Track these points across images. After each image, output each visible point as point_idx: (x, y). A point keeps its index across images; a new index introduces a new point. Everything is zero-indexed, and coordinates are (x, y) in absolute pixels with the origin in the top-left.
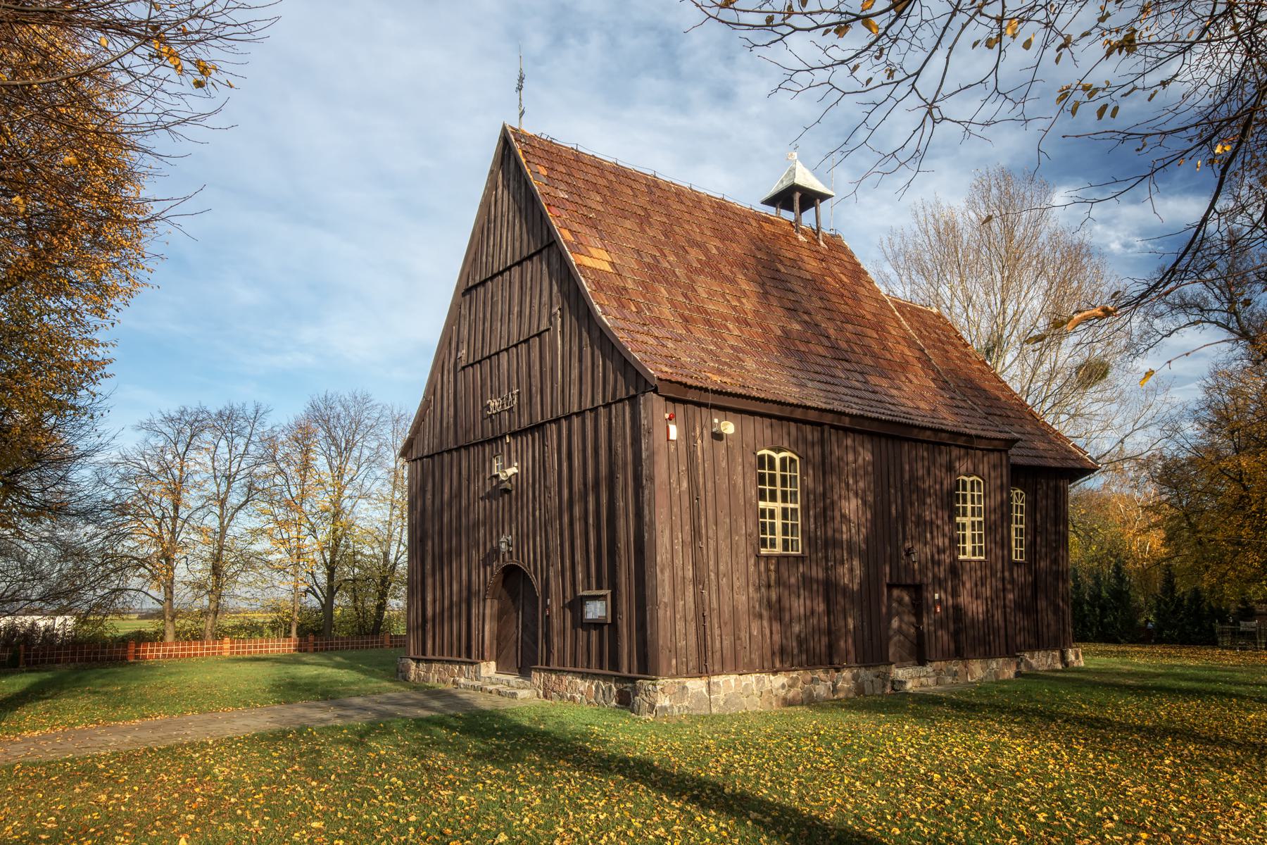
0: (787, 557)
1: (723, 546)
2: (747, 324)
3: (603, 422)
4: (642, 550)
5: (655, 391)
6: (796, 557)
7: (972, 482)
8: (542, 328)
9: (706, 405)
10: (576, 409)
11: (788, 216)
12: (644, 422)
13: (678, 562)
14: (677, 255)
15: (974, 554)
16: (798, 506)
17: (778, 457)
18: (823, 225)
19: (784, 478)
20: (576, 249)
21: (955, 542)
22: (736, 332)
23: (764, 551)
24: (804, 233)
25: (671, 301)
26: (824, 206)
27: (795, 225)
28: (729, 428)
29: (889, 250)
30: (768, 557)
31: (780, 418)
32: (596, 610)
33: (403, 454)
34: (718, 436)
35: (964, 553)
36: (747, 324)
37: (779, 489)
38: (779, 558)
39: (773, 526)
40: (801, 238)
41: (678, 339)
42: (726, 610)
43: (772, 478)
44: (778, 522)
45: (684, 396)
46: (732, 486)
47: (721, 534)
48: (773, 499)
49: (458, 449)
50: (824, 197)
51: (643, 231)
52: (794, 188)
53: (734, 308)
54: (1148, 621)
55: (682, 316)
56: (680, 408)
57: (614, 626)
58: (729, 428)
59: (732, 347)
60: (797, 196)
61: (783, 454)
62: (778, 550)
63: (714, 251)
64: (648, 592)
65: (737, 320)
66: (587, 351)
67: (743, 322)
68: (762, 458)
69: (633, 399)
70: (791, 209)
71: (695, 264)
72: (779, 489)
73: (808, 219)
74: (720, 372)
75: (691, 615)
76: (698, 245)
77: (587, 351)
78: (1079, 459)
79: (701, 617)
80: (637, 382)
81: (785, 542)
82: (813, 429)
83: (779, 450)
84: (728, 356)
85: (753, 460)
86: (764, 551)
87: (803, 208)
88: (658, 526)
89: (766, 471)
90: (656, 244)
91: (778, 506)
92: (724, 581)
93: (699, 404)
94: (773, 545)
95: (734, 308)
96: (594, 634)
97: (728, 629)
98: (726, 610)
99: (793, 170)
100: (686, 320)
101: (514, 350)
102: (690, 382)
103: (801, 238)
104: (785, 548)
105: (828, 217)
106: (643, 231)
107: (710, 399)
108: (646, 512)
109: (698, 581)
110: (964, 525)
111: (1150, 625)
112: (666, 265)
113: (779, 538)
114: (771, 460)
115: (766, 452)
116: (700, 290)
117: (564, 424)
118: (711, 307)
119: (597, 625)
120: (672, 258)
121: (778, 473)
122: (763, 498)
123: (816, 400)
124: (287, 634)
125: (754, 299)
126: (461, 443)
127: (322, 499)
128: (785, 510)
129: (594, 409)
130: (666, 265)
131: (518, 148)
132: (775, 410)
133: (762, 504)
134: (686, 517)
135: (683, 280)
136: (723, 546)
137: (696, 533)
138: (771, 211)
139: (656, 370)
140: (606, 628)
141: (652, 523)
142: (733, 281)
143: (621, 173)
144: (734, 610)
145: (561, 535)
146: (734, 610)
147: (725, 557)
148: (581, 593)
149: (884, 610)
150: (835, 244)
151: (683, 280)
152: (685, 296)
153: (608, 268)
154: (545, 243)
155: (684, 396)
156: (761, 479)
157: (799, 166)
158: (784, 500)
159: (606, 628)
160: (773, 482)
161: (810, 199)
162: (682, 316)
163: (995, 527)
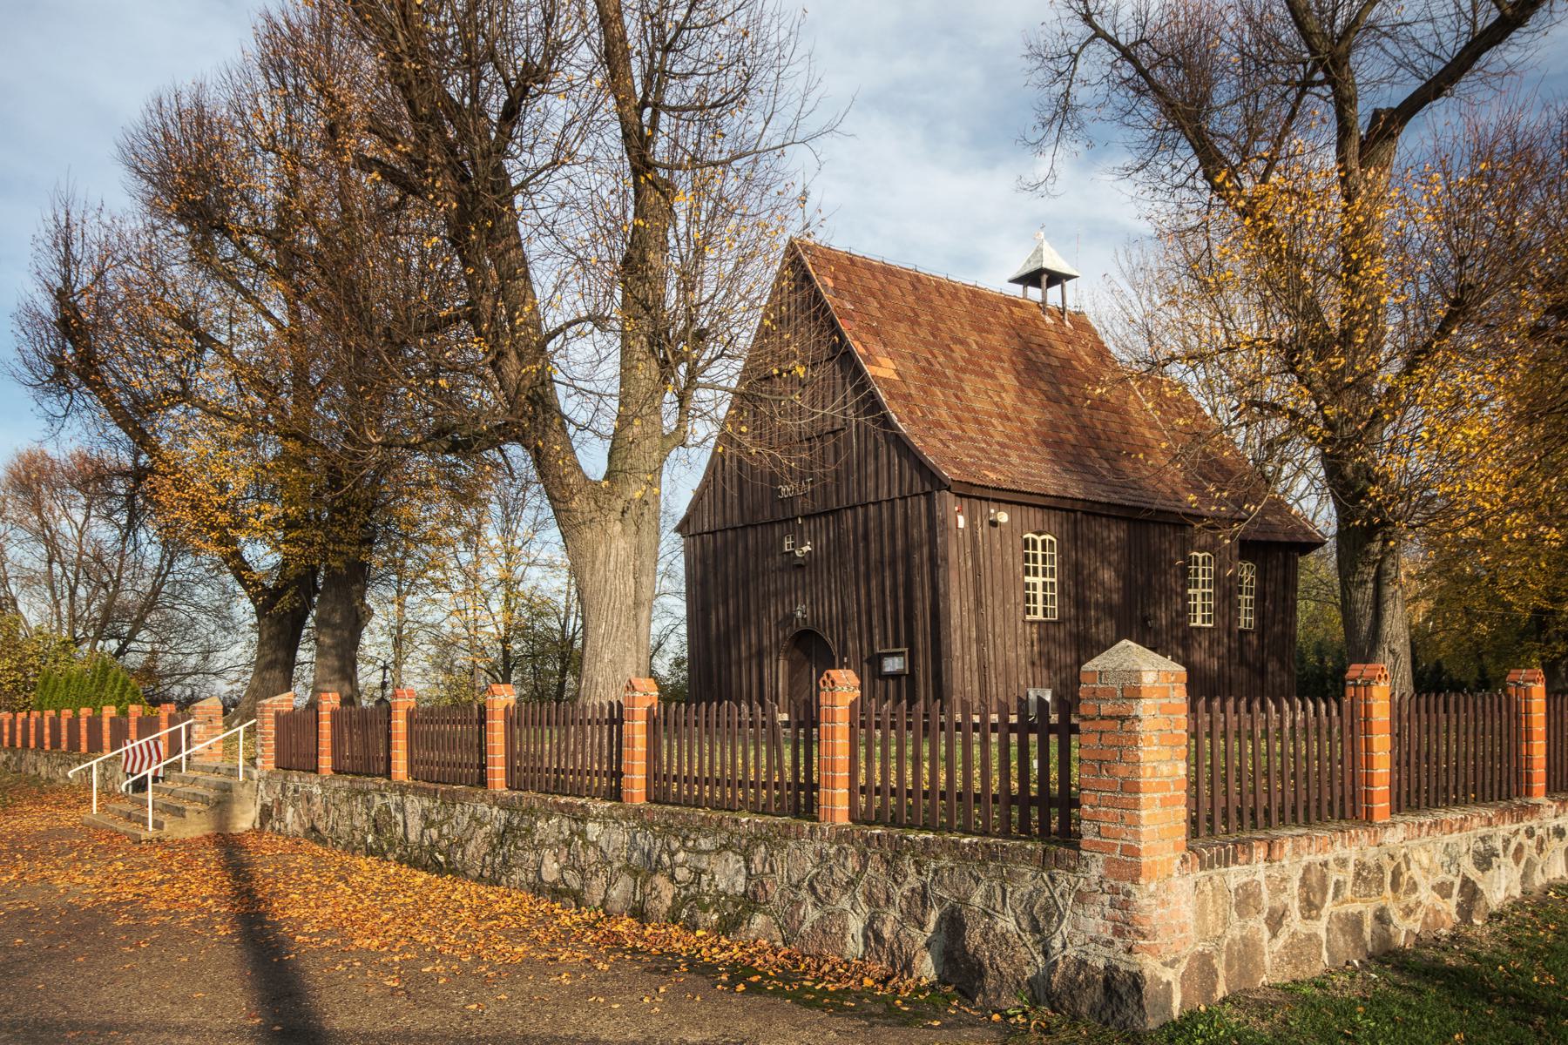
1: (998, 612)
2: (1009, 419)
3: (899, 511)
4: (937, 618)
5: (949, 489)
8: (837, 427)
9: (987, 499)
10: (872, 499)
12: (939, 514)
13: (966, 625)
14: (945, 356)
16: (1055, 580)
17: (1039, 539)
18: (1069, 302)
19: (1044, 557)
20: (868, 360)
21: (1185, 611)
22: (1000, 428)
23: (1028, 618)
24: (1051, 315)
25: (946, 404)
27: (1042, 306)
28: (1003, 517)
29: (1125, 265)
30: (1032, 622)
31: (1041, 507)
32: (893, 665)
33: (679, 529)
34: (994, 524)
36: (1009, 419)
37: (1040, 565)
40: (1048, 320)
41: (956, 438)
42: (1000, 663)
43: (1035, 556)
45: (971, 493)
46: (1004, 565)
47: (997, 603)
48: (1036, 574)
49: (745, 527)
50: (1069, 277)
51: (915, 333)
52: (1042, 271)
53: (996, 404)
55: (956, 417)
56: (965, 501)
57: (912, 677)
58: (1003, 517)
59: (999, 443)
60: (1045, 278)
62: (1040, 616)
63: (974, 346)
64: (944, 648)
65: (1000, 416)
66: (883, 451)
67: (1005, 418)
68: (1027, 541)
69: (929, 495)
71: (961, 363)
72: (1040, 565)
74: (993, 469)
75: (975, 667)
76: (962, 342)
77: (883, 451)
78: (1307, 533)
79: (983, 668)
80: (933, 481)
81: (1045, 610)
82: (1075, 517)
83: (1039, 533)
84: (997, 452)
85: (1019, 543)
86: (1028, 618)
87: (1050, 284)
88: (952, 596)
90: (926, 343)
91: (1039, 580)
92: (998, 641)
93: (980, 498)
94: (1035, 613)
95: (996, 404)
96: (891, 683)
97: (1001, 679)
98: (1000, 663)
99: (1039, 251)
100: (959, 420)
102: (974, 481)
103: (1048, 320)
105: (1074, 297)
106: (915, 333)
107: (991, 494)
108: (941, 585)
109: (979, 640)
110: (1035, 585)
112: (938, 367)
113: (1040, 606)
114: (1034, 541)
116: (967, 389)
117: (860, 510)
118: (977, 406)
119: (896, 676)
120: (941, 359)
121: (1039, 552)
122: (1027, 573)
123: (1075, 491)
125: (1012, 395)
126: (748, 520)
127: (492, 571)
129: (891, 501)
130: (938, 367)
131: (824, 283)
132: (1041, 501)
133: (1027, 579)
134: (971, 590)
135: (954, 381)
136: (998, 612)
137: (979, 602)
138: (1017, 291)
139: (949, 473)
140: (904, 679)
141: (947, 594)
142: (993, 377)
143: (888, 271)
144: (1006, 664)
145: (858, 604)
146: (1006, 664)
147: (999, 622)
148: (878, 650)
150: (1080, 321)
151: (954, 381)
152: (957, 397)
153: (896, 377)
155: (971, 493)
156: (1027, 557)
157: (1046, 246)
158: (1044, 575)
159: (904, 679)
160: (1035, 561)
161: (1056, 278)
162: (956, 417)
163: (1226, 592)
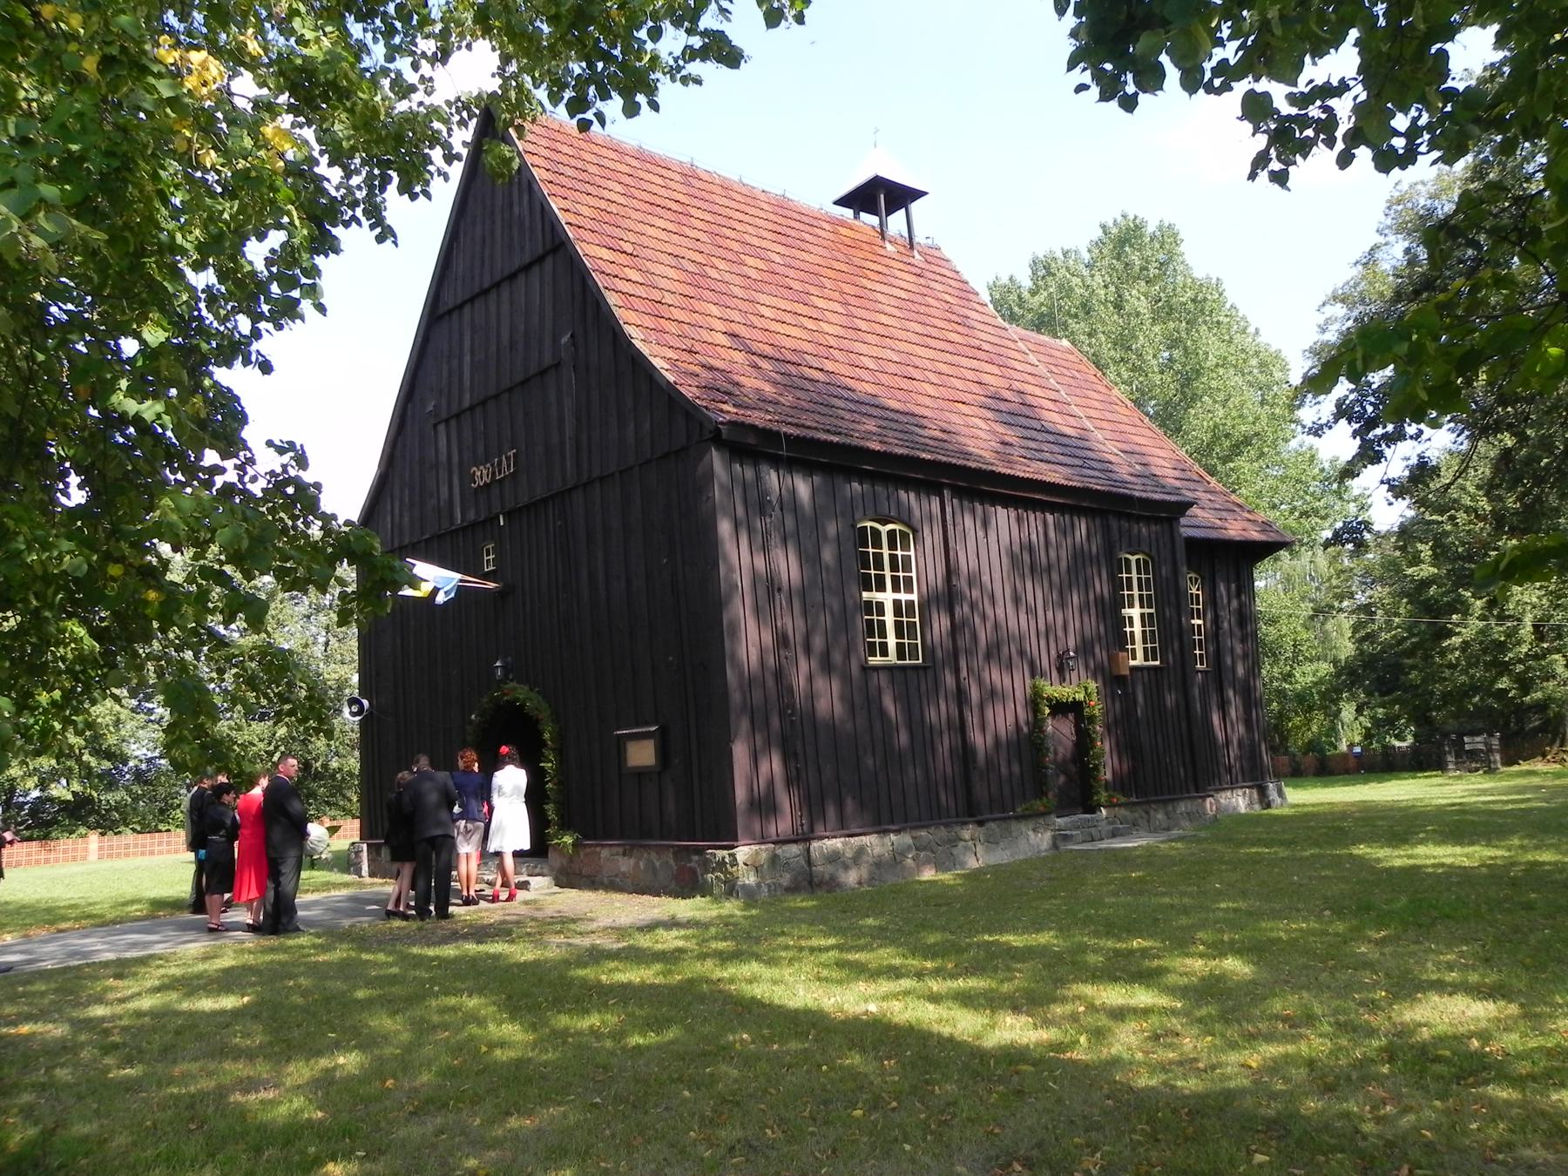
0: (904, 668)
6: (915, 668)
7: (1138, 561)
11: (869, 219)
15: (1146, 659)
26: (915, 207)
35: (1134, 658)
38: (890, 669)
39: (882, 624)
44: (889, 618)
54: (1351, 746)
61: (890, 527)
62: (892, 658)
70: (874, 211)
73: (897, 221)
83: (884, 523)
89: (871, 550)
101: (506, 395)
104: (901, 656)
111: (1358, 750)
113: (892, 641)
115: (869, 524)
124: (359, 224)
128: (897, 603)
133: (865, 595)
149: (229, 1002)
150: (934, 258)
154: (549, 245)
158: (896, 589)
